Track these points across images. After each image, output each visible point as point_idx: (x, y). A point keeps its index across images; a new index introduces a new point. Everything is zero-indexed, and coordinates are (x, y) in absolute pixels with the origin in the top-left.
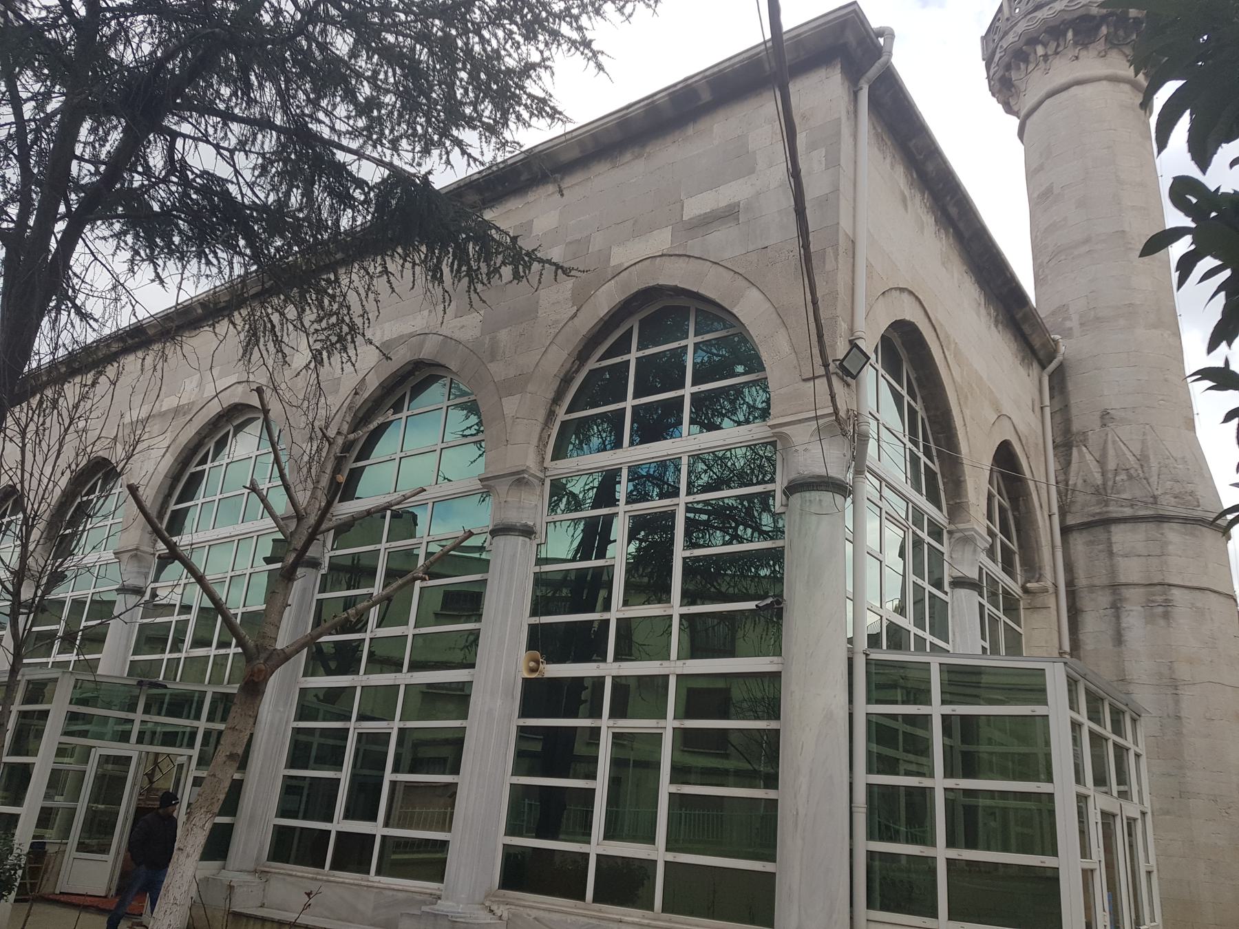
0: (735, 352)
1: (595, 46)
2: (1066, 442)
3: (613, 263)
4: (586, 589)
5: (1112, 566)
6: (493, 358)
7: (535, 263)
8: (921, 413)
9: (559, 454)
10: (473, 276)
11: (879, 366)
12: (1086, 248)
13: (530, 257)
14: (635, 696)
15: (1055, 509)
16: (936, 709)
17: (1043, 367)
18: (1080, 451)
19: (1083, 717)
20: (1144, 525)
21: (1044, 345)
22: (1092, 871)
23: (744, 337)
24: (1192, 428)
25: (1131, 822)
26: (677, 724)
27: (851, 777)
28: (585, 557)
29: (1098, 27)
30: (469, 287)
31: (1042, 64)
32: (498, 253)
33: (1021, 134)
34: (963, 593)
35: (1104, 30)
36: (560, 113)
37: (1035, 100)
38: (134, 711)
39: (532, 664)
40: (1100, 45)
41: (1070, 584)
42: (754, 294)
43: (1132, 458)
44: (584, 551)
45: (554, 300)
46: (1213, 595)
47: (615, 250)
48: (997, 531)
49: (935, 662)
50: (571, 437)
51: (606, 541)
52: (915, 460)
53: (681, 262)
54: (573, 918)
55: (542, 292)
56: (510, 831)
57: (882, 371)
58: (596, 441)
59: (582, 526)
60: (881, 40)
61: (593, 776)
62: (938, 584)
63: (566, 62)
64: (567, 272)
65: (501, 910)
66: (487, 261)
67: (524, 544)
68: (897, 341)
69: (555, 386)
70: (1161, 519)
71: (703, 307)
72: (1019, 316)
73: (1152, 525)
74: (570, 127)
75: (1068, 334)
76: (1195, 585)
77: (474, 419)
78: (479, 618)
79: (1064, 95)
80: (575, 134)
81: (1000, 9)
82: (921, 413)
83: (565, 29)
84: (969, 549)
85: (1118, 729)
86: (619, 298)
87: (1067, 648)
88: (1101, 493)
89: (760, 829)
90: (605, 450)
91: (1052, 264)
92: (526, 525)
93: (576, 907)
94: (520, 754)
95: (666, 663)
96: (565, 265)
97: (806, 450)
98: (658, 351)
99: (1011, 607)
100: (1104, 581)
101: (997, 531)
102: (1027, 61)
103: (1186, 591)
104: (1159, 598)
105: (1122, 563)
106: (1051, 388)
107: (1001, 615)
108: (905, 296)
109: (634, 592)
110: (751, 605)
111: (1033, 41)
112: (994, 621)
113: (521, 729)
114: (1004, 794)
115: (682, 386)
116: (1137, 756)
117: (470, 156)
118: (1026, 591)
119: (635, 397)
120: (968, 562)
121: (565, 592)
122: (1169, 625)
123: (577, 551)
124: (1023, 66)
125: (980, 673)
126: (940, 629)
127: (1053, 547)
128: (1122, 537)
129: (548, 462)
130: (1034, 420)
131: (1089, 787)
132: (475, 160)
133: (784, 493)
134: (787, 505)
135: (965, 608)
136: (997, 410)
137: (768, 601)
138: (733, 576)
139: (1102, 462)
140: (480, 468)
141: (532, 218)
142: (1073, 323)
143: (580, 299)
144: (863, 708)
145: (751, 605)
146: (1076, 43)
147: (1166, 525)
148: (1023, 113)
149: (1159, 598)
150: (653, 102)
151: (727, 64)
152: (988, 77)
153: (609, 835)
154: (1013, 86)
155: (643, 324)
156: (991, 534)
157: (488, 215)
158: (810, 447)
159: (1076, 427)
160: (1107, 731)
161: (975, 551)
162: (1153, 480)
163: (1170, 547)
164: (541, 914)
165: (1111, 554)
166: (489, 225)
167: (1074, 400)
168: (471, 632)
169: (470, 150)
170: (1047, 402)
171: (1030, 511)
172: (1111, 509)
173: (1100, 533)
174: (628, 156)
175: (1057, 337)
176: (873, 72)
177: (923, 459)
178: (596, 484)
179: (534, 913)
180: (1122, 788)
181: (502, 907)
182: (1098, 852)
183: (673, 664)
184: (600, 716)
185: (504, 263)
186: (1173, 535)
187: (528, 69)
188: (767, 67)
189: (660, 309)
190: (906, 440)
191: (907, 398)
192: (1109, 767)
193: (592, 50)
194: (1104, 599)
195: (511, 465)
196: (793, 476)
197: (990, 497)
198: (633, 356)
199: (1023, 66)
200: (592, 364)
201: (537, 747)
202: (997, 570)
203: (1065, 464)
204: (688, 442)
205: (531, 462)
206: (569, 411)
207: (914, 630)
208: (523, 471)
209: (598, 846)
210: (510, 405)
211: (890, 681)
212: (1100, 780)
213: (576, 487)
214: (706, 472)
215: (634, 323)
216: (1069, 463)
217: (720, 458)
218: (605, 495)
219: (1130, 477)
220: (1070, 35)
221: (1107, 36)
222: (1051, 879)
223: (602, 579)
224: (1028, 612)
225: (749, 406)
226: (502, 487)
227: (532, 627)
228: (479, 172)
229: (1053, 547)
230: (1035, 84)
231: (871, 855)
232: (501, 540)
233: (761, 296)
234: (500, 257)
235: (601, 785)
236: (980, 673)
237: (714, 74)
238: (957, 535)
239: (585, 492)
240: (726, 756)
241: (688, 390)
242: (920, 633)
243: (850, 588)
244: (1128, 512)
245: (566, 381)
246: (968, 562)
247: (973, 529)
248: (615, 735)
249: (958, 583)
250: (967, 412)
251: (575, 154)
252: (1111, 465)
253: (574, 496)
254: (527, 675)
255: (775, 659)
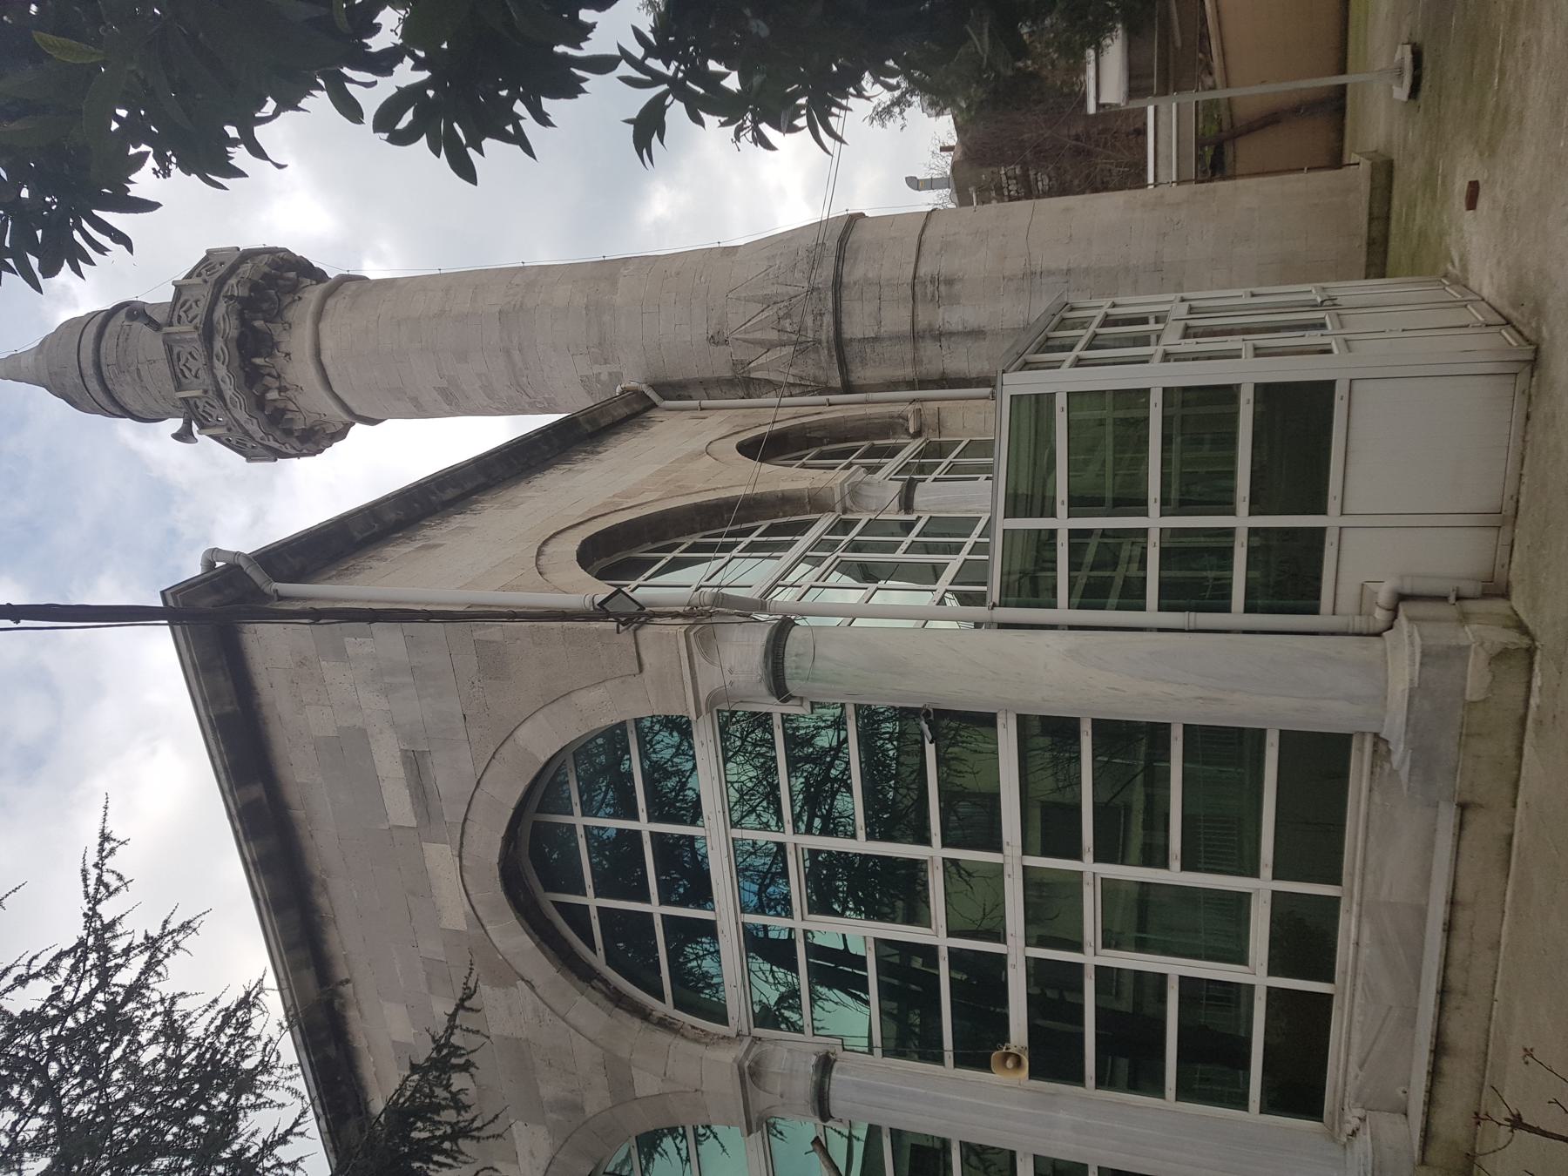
0: (599, 762)
1: (155, 932)
2: (744, 384)
3: (463, 926)
4: (906, 977)
5: (890, 339)
6: (577, 1108)
7: (453, 1040)
8: (697, 538)
9: (718, 1014)
10: (459, 1132)
11: (633, 584)
12: (516, 355)
13: (444, 1046)
14: (1050, 908)
15: (823, 399)
16: (1062, 523)
17: (654, 406)
18: (755, 369)
19: (1070, 357)
20: (845, 304)
21: (627, 404)
22: (1256, 349)
23: (580, 751)
24: (734, 250)
25: (1191, 310)
26: (1088, 856)
27: (1150, 630)
28: (863, 984)
29: (255, 330)
30: (473, 1138)
31: (289, 394)
32: (432, 1095)
33: (373, 422)
34: (919, 498)
35: (259, 324)
36: (248, 994)
37: (331, 402)
38: (1073, 533)
39: (1010, 1064)
40: (276, 329)
41: (911, 385)
42: (523, 733)
43: (766, 313)
44: (853, 985)
45: (505, 1013)
46: (928, 232)
47: (445, 924)
48: (846, 462)
49: (1003, 524)
50: (698, 996)
51: (844, 956)
52: (753, 547)
53: (472, 829)
54: (1357, 1010)
55: (493, 1031)
56: (1241, 1102)
57: (640, 581)
58: (708, 964)
59: (823, 990)
60: (219, 564)
61: (1162, 978)
62: (907, 527)
63: (175, 977)
64: (469, 994)
65: (1352, 1117)
66: (438, 1108)
67: (842, 1070)
68: (605, 562)
69: (624, 1016)
70: (837, 284)
71: (535, 804)
72: (589, 428)
73: (845, 294)
74: (271, 981)
75: (616, 377)
76: (915, 250)
77: (667, 1143)
78: (945, 1144)
79: (330, 371)
80: (282, 975)
81: (216, 438)
82: (697, 538)
83: (125, 977)
84: (866, 491)
85: (1084, 324)
86: (511, 919)
87: (987, 391)
88: (802, 348)
89: (1224, 749)
90: (718, 952)
91: (531, 393)
92: (816, 1066)
93: (1341, 1008)
94: (1133, 1086)
95: (1007, 870)
96: (459, 995)
97: (731, 672)
98: (589, 871)
99: (940, 450)
100: (908, 347)
101: (846, 462)
102: (284, 411)
103: (922, 259)
104: (930, 288)
105: (888, 327)
106: (679, 398)
107: (946, 461)
108: (548, 550)
109: (916, 913)
110: (930, 750)
111: (260, 403)
112: (953, 468)
113: (1100, 1083)
114: (1165, 462)
115: (638, 833)
116: (1114, 306)
117: (289, 1132)
118: (918, 434)
119: (647, 900)
120: (884, 488)
121: (915, 1019)
122: (961, 280)
123: (857, 998)
124: (289, 416)
125: (1016, 495)
126: (964, 525)
127: (867, 402)
128: (856, 327)
129: (729, 1030)
130: (714, 419)
131: (1154, 350)
132: (296, 1123)
133: (785, 701)
134: (802, 699)
135: (936, 497)
136: (700, 454)
137: (925, 727)
138: (896, 789)
139: (770, 346)
140: (732, 1135)
141: (389, 1040)
142: (604, 371)
143: (506, 975)
144: (1063, 613)
145: (930, 750)
146: (270, 355)
147: (845, 280)
148: (347, 418)
149: (930, 288)
150: (254, 864)
151: (218, 761)
152: (298, 456)
153: (1240, 958)
154: (312, 428)
155: (550, 887)
156: (848, 467)
157: (378, 1105)
158: (727, 666)
159: (727, 373)
160: (1086, 334)
161: (868, 484)
162: (791, 291)
163: (870, 275)
164: (1354, 1059)
165: (876, 339)
166: (392, 1108)
167: (694, 373)
168: (965, 1161)
169: (281, 1131)
170: (695, 403)
171: (822, 426)
172: (824, 338)
173: (852, 351)
174: (322, 901)
175: (618, 389)
176: (258, 576)
177: (753, 537)
178: (767, 967)
179: (1353, 1068)
180: (1152, 320)
181: (1348, 1117)
182: (1233, 343)
183: (1009, 860)
184: (1081, 966)
185: (447, 1087)
186: (855, 272)
187: (172, 1032)
188: (229, 709)
189: (532, 863)
190: (728, 556)
191: (676, 553)
192: (1128, 332)
193: (162, 937)
194: (929, 349)
195: (731, 1087)
196: (763, 689)
197: (804, 466)
198: (592, 901)
199: (289, 416)
200: (598, 961)
201: (1123, 1063)
202: (891, 465)
203: (771, 386)
204: (715, 839)
205: (728, 1056)
206: (661, 998)
207: (964, 554)
208: (740, 1068)
209: (1255, 973)
210: (646, 1084)
211: (1028, 584)
212: (1144, 341)
213: (772, 996)
214: (759, 816)
215: (548, 899)
216: (769, 382)
217: (742, 796)
218: (777, 952)
219: (788, 315)
220: (259, 361)
221: (266, 321)
222: (1265, 392)
223: (897, 959)
224: (944, 432)
225: (676, 755)
226: (762, 1101)
227: (959, 1062)
228: (318, 1119)
229: (867, 402)
230: (313, 402)
231: (1249, 609)
232: (837, 1105)
233: (528, 724)
234: (439, 1091)
235: (1175, 967)
236: (1016, 495)
237: (228, 779)
238: (848, 503)
239: (777, 983)
240: (1128, 808)
241: (644, 826)
242: (967, 548)
243: (910, 624)
244: (828, 319)
245: (618, 999)
246: (884, 488)
247: (842, 484)
248: (1105, 945)
249: (907, 503)
250: (699, 486)
251: (309, 976)
252: (773, 335)
253: (782, 999)
254: (1026, 1072)
255: (1000, 722)
